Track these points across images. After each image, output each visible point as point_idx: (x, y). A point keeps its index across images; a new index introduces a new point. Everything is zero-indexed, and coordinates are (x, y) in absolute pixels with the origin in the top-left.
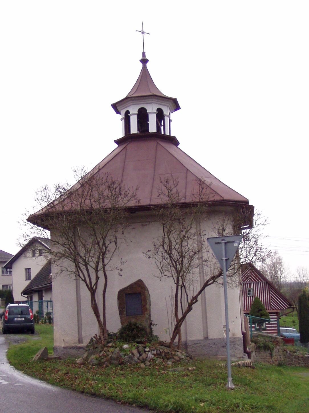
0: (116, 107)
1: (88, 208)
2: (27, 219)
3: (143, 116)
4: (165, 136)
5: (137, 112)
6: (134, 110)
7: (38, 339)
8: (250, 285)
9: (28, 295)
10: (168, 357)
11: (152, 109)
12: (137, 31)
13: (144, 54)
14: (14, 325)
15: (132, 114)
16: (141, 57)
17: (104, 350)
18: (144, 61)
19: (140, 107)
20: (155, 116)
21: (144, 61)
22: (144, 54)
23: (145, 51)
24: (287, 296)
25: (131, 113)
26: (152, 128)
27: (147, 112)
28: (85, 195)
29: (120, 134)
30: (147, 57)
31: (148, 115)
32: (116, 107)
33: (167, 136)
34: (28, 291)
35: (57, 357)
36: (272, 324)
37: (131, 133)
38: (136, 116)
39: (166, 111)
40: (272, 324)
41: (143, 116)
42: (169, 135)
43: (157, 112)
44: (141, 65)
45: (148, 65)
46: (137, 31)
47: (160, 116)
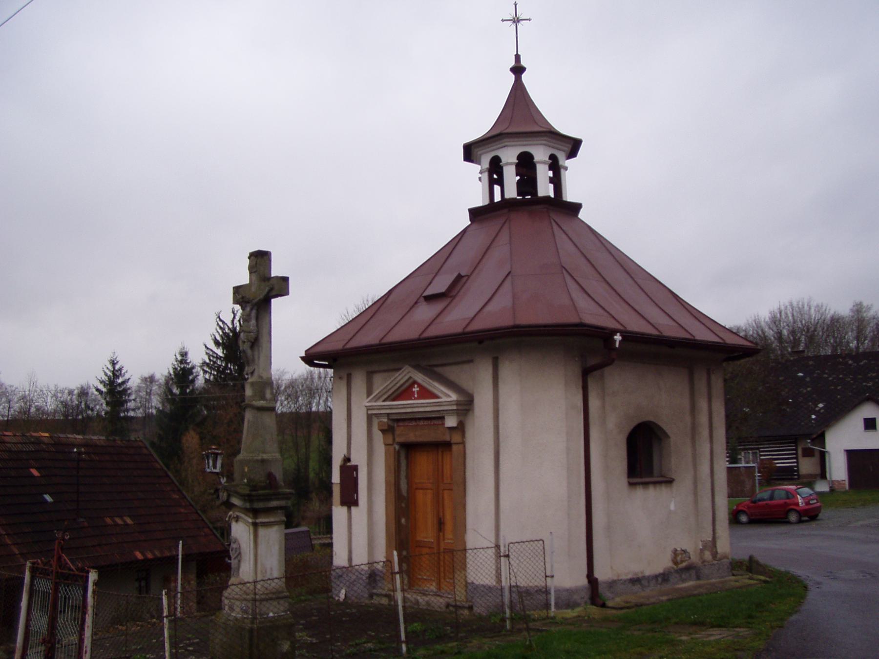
0: (470, 152)
2: (285, 529)
3: (526, 164)
6: (509, 156)
7: (680, 636)
9: (349, 464)
10: (240, 649)
11: (540, 154)
13: (518, 57)
14: (500, 144)
15: (508, 164)
16: (512, 63)
17: (502, 554)
18: (518, 70)
21: (518, 70)
22: (518, 57)
24: (744, 337)
26: (545, 189)
27: (535, 160)
30: (523, 63)
34: (361, 349)
41: (526, 164)
44: (512, 77)
45: (525, 77)
47: (555, 166)
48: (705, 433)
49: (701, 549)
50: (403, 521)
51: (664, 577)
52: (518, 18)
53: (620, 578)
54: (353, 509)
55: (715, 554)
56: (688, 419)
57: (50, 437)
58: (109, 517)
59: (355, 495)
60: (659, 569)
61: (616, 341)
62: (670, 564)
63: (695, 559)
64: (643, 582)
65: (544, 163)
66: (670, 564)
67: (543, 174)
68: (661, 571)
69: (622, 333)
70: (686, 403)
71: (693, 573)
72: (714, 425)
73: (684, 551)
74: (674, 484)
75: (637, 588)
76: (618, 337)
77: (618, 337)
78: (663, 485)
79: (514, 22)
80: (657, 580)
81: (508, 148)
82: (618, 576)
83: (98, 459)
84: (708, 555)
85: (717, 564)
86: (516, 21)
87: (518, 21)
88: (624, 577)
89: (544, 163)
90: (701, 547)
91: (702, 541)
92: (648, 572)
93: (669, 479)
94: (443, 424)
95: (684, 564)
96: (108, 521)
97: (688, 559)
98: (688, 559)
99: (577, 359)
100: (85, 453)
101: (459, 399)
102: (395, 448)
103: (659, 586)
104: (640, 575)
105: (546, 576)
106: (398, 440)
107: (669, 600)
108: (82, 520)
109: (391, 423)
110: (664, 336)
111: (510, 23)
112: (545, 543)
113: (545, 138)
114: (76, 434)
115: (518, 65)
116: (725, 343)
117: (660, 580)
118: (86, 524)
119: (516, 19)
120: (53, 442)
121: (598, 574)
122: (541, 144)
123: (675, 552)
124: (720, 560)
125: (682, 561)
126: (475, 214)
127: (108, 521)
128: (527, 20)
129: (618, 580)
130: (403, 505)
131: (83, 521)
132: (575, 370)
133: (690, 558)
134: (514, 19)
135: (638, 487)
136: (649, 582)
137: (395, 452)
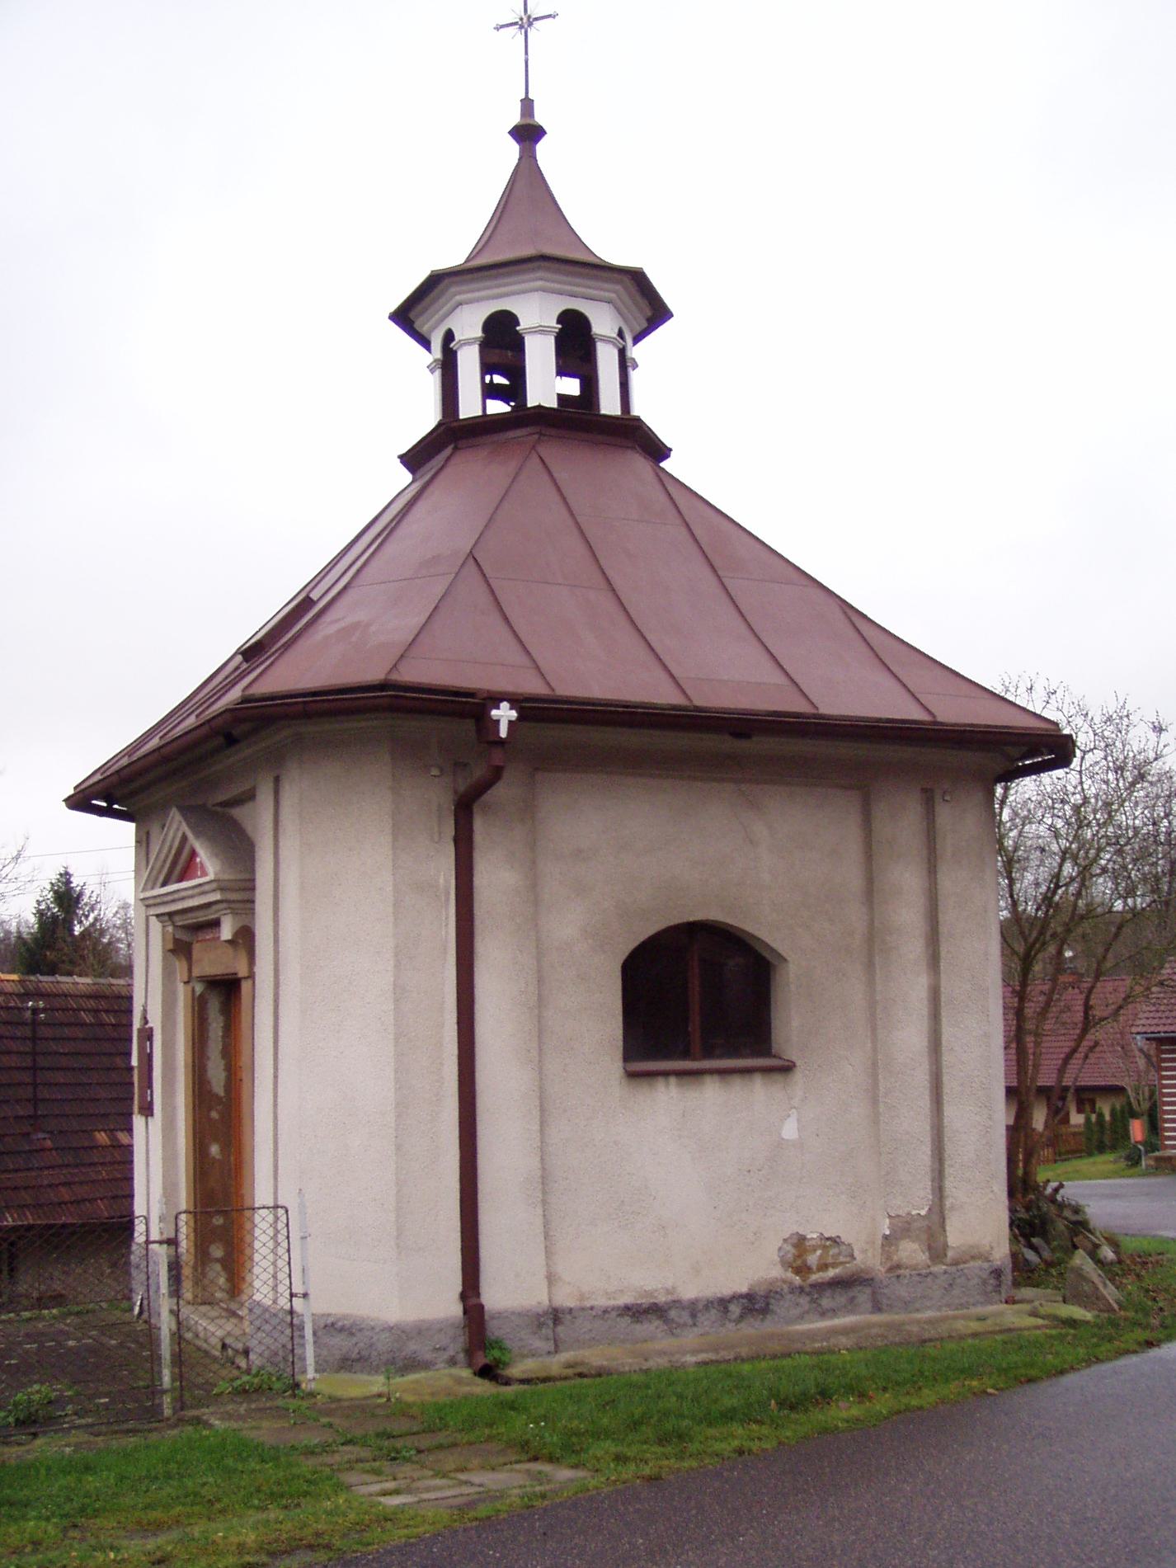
0: (404, 317)
1: (1029, 988)
4: (461, 423)
5: (479, 333)
6: (468, 324)
8: (1169, 1136)
12: (499, 28)
13: (527, 105)
16: (515, 119)
18: (528, 134)
19: (493, 310)
20: (550, 343)
21: (528, 134)
22: (527, 105)
23: (530, 97)
25: (458, 337)
28: (1073, 894)
29: (426, 418)
30: (540, 118)
31: (524, 338)
32: (404, 317)
33: (468, 422)
35: (22, 1226)
36: (124, 756)
37: (529, 405)
38: (553, 341)
39: (603, 322)
40: (124, 756)
42: (619, 413)
43: (560, 326)
44: (512, 151)
45: (542, 148)
46: (499, 28)
48: (913, 948)
49: (886, 1237)
50: (215, 1150)
51: (755, 1304)
52: (529, 17)
53: (588, 1304)
54: (149, 1118)
55: (937, 1251)
56: (855, 915)
57: (19, 981)
58: (105, 1131)
59: (149, 1092)
60: (735, 1280)
61: (498, 722)
62: (777, 1272)
63: (867, 1258)
64: (673, 1314)
65: (541, 330)
66: (777, 1272)
67: (540, 355)
68: (744, 1289)
69: (515, 701)
70: (851, 875)
71: (863, 1296)
72: (943, 930)
73: (835, 1241)
74: (798, 1076)
75: (653, 1326)
76: (504, 714)
77: (504, 714)
78: (673, 1080)
79: (521, 27)
80: (726, 1310)
81: (464, 306)
82: (582, 1297)
83: (113, 1021)
84: (911, 1252)
85: (945, 1272)
86: (525, 23)
87: (530, 24)
88: (601, 1302)
89: (541, 330)
90: (888, 1233)
91: (890, 1217)
92: (690, 1291)
93: (787, 1064)
94: (219, 938)
95: (831, 1273)
96: (102, 1138)
97: (848, 1259)
98: (848, 1259)
99: (435, 772)
100: (44, 1010)
101: (226, 877)
102: (193, 991)
103: (731, 1326)
104: (662, 1299)
105: (292, 1295)
106: (196, 972)
107: (698, 1364)
108: (41, 1135)
109: (181, 935)
110: (822, 717)
111: (514, 29)
112: (289, 1212)
113: (539, 274)
114: (41, 975)
115: (529, 121)
116: (935, 723)
117: (736, 1310)
118: (49, 1143)
119: (525, 20)
120: (22, 991)
121: (494, 1297)
122: (536, 290)
123: (800, 1242)
124: (955, 1263)
125: (824, 1267)
126: (414, 459)
127: (102, 1138)
128: (549, 16)
129: (583, 1309)
130: (214, 1115)
131: (45, 1139)
132: (434, 795)
133: (852, 1257)
134: (521, 19)
135: (660, 1083)
136: (693, 1316)
137: (193, 999)
